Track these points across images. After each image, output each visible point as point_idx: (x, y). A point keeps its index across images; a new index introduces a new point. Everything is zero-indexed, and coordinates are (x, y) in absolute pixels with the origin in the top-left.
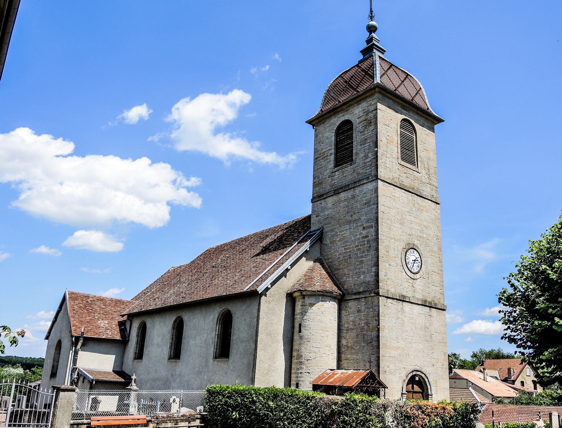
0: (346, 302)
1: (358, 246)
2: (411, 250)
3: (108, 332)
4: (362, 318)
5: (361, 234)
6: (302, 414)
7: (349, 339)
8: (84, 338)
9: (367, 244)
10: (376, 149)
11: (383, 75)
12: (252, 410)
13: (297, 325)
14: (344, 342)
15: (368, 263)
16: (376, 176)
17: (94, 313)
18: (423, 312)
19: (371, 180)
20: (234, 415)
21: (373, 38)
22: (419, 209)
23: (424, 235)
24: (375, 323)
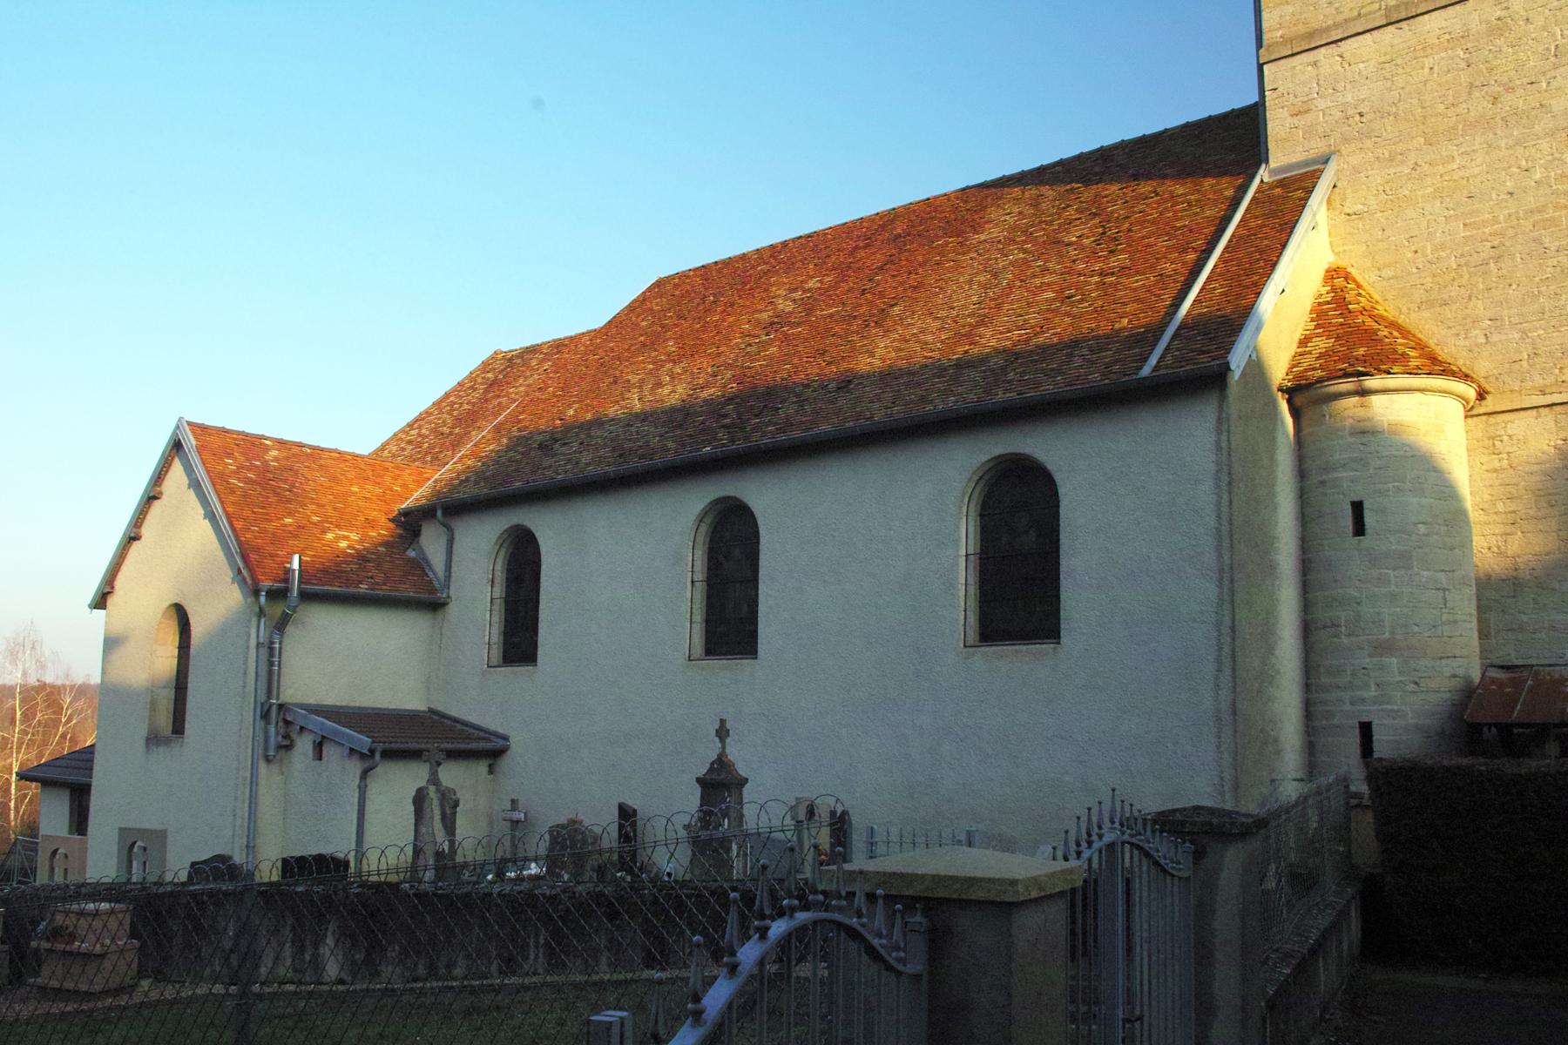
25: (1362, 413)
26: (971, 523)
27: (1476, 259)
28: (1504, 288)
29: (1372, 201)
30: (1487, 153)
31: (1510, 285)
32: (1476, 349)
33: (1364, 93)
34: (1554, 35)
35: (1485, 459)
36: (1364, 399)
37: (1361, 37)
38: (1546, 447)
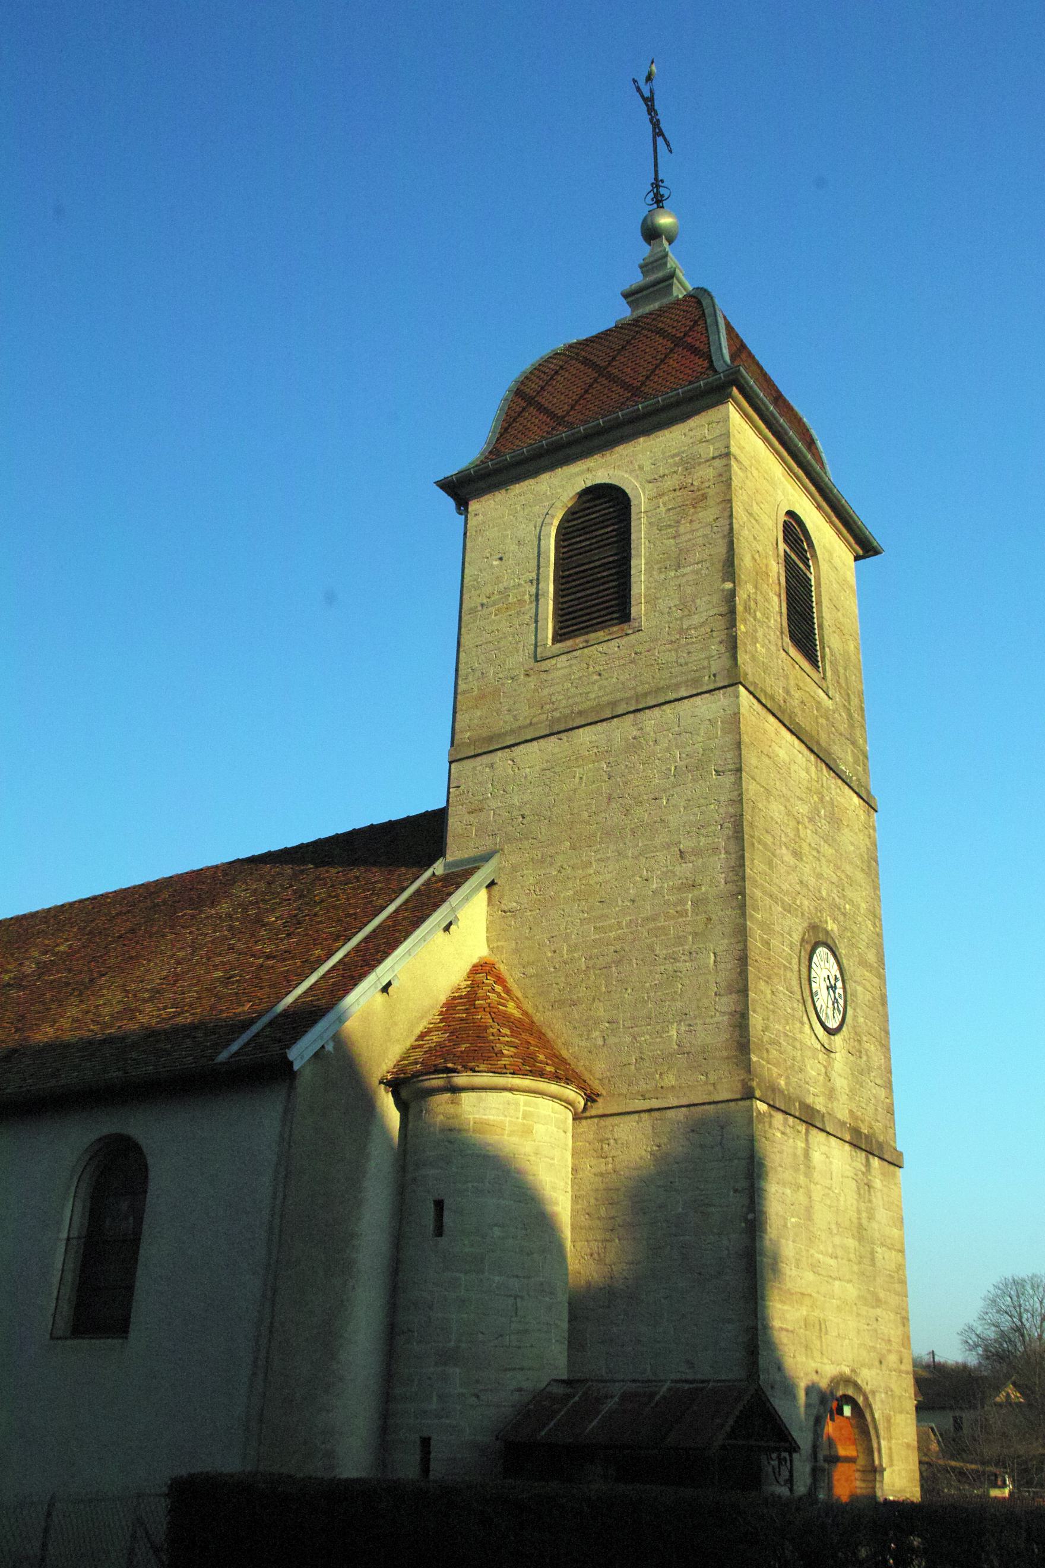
1: (654, 918)
4: (677, 1184)
25: (451, 1109)
26: (79, 1205)
27: (601, 963)
28: (621, 992)
29: (524, 900)
30: (618, 860)
31: (626, 989)
32: (594, 1051)
33: (527, 797)
34: (674, 757)
35: (594, 1162)
36: (455, 1096)
37: (529, 744)
38: (644, 1153)
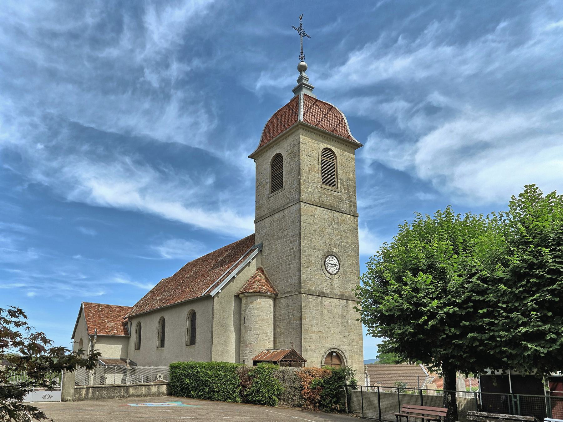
0: (279, 300)
1: (287, 256)
2: (330, 256)
3: (115, 331)
5: (289, 246)
6: (230, 378)
7: (282, 326)
8: (97, 336)
9: (293, 255)
10: (299, 177)
11: (307, 111)
12: (198, 377)
13: (243, 319)
14: (278, 329)
15: (294, 269)
16: (299, 199)
17: (104, 318)
18: (340, 304)
19: (296, 203)
20: (187, 381)
21: (303, 78)
22: (338, 223)
23: (343, 244)
24: (299, 314)
